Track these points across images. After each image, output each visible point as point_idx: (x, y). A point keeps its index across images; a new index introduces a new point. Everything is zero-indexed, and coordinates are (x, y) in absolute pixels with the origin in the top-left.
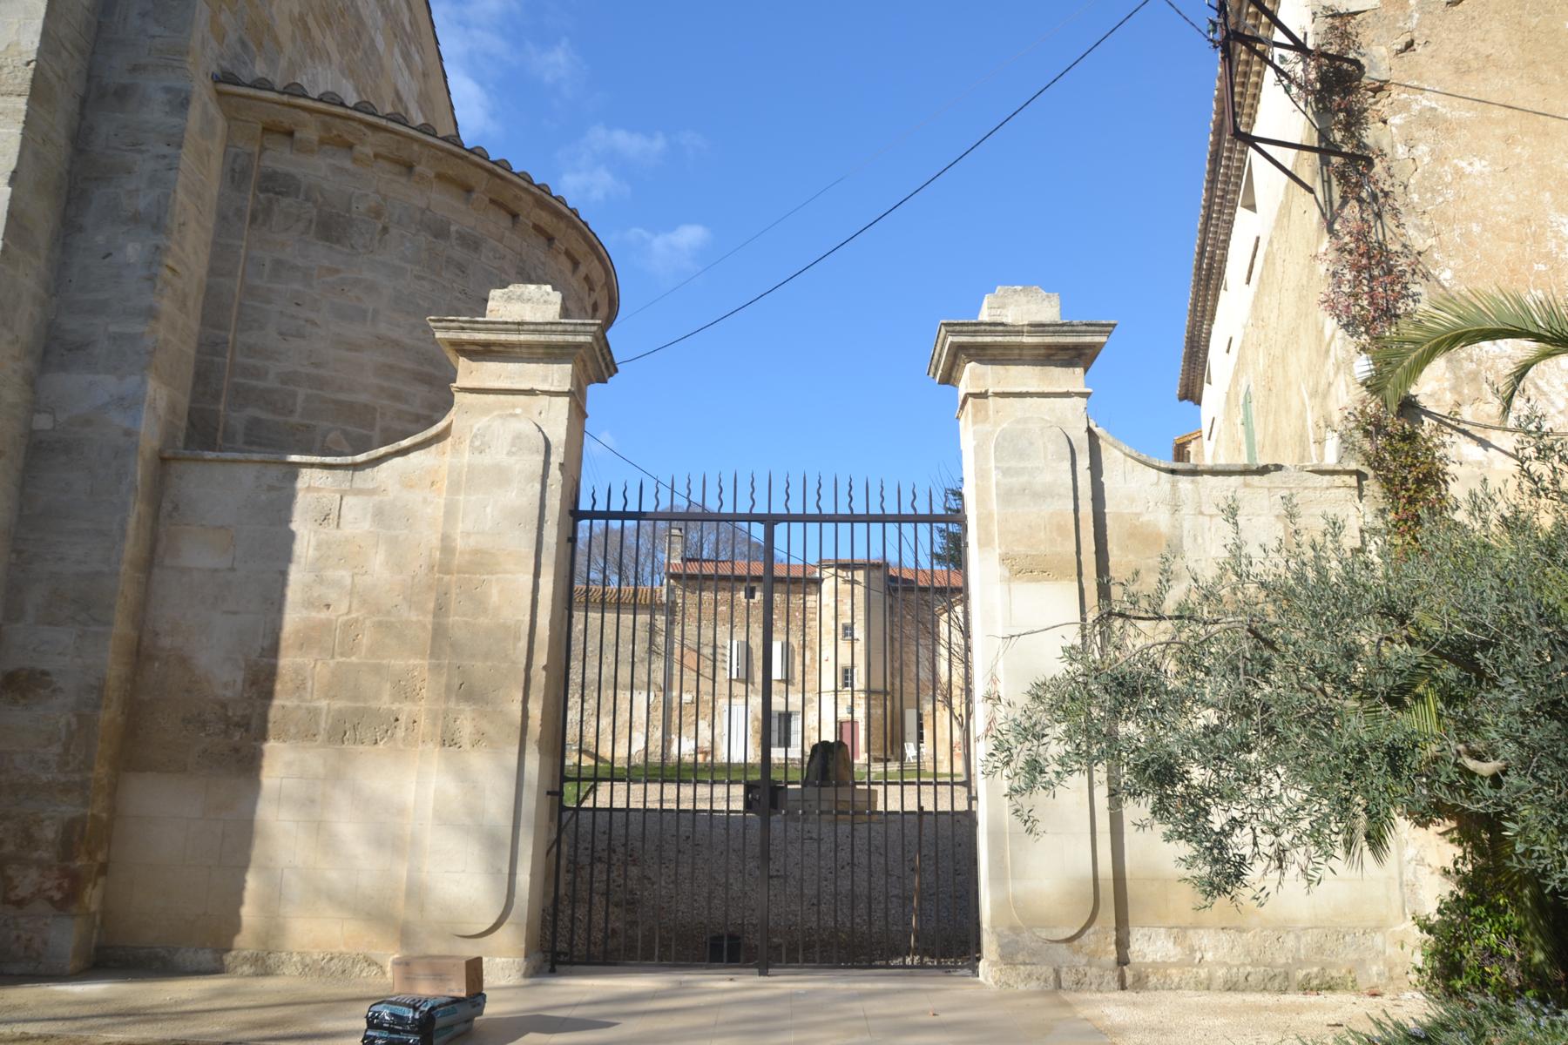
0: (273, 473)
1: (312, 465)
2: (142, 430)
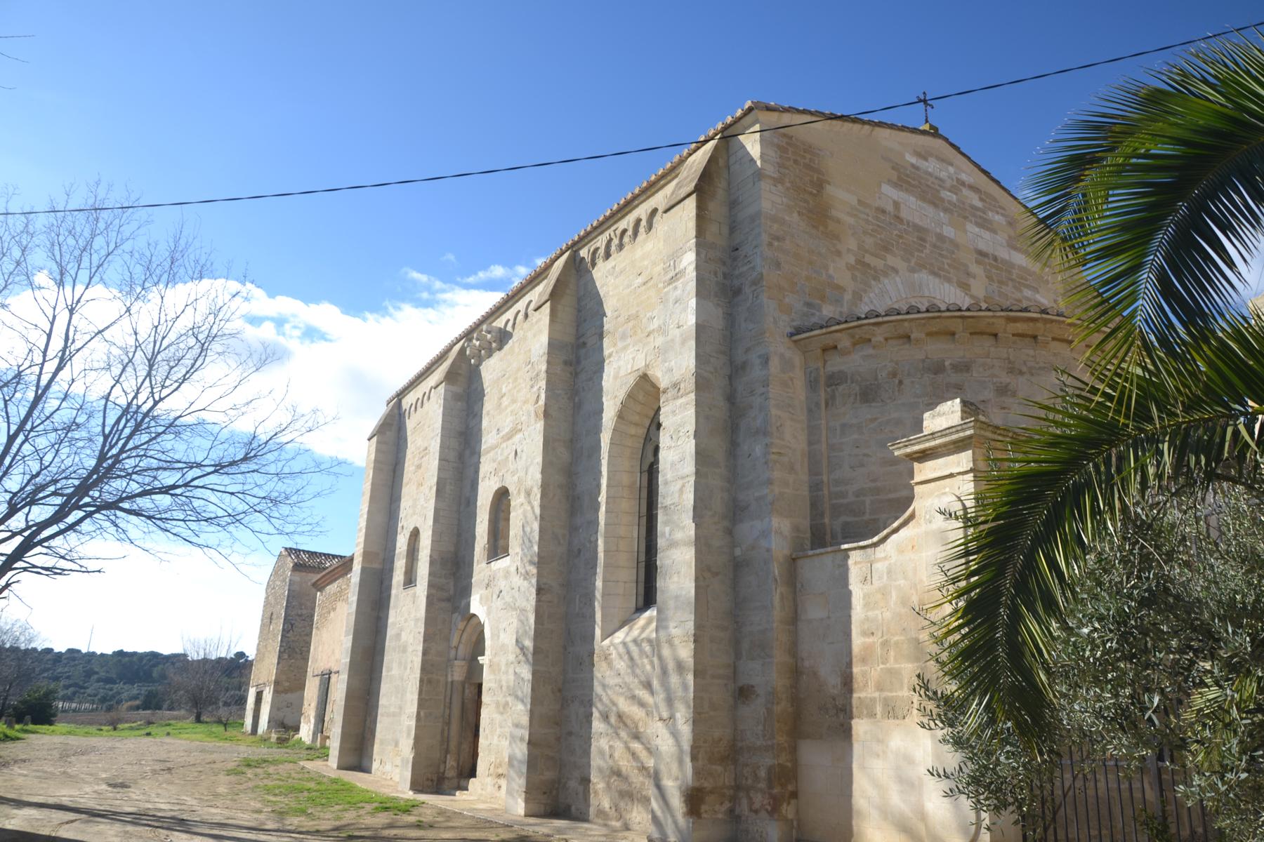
0: (839, 556)
1: (855, 549)
2: (774, 547)
